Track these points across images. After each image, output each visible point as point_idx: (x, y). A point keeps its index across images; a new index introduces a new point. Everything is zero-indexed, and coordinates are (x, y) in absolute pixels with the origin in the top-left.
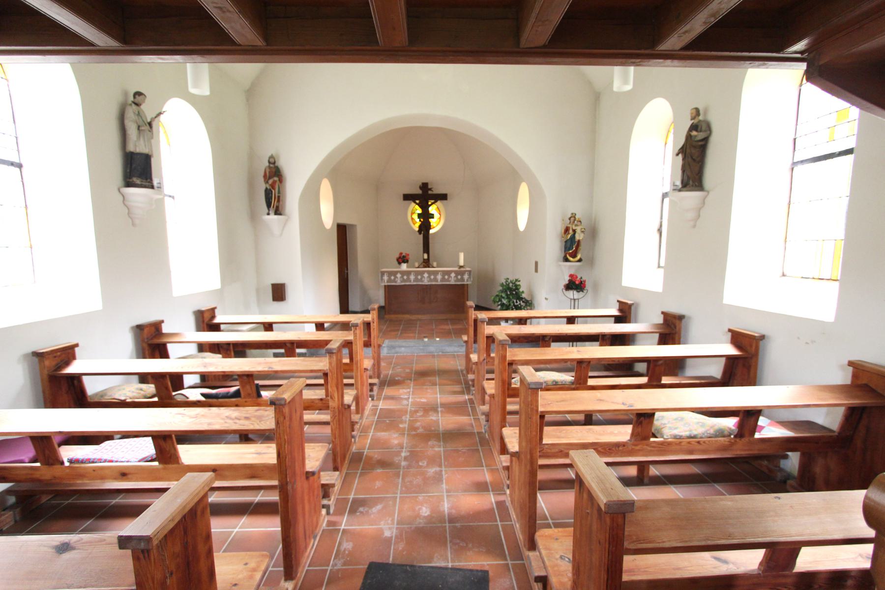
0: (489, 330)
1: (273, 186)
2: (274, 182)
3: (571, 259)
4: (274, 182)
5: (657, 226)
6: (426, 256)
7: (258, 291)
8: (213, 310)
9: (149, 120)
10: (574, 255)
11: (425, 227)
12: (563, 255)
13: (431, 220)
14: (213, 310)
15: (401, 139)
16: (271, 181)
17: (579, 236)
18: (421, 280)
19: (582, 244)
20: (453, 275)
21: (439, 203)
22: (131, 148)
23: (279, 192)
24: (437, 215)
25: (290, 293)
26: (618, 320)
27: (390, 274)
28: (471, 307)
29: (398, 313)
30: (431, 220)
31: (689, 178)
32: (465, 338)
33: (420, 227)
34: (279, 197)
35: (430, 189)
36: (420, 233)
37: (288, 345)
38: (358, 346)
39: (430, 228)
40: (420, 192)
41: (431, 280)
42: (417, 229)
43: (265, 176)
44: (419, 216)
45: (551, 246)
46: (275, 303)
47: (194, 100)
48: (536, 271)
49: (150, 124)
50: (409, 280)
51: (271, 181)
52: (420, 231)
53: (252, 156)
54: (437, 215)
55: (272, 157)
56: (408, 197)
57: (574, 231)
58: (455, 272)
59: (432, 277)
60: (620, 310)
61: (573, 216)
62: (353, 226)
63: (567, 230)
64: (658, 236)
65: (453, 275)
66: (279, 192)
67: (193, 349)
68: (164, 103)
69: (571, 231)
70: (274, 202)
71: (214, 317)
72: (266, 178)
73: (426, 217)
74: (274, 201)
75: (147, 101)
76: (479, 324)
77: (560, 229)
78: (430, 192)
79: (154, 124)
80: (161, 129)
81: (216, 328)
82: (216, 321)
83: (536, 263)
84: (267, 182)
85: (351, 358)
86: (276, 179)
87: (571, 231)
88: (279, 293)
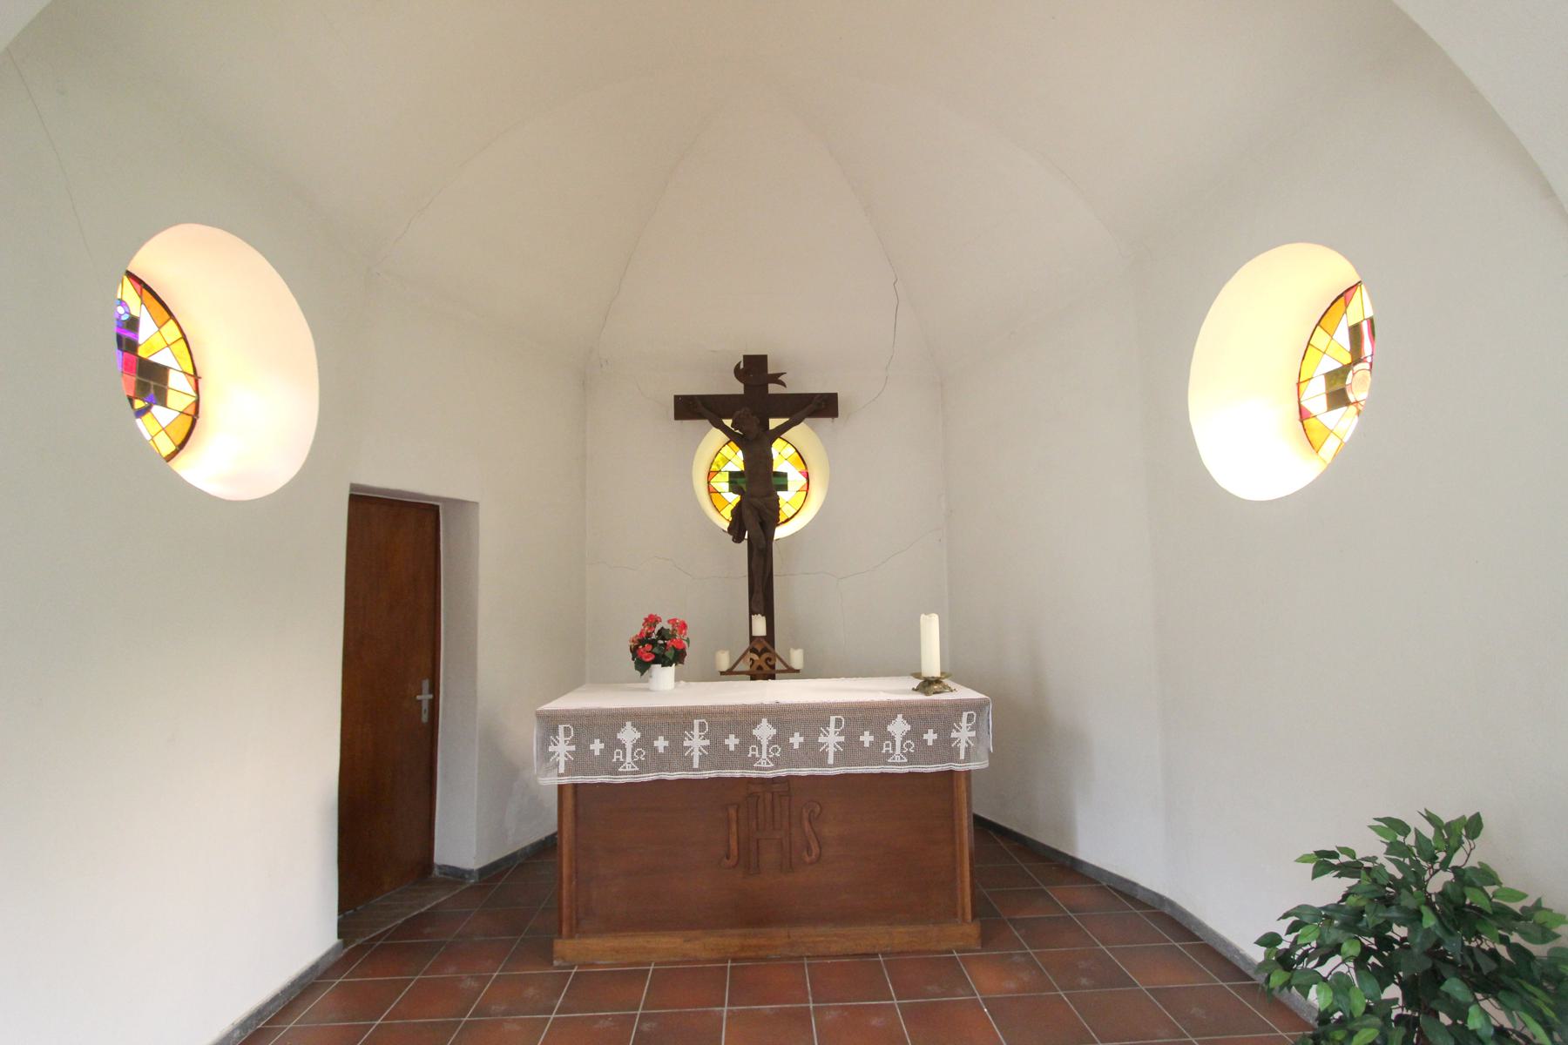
20: (899, 727)
33: (737, 512)
35: (776, 379)
36: (738, 539)
39: (776, 522)
40: (738, 388)
41: (789, 757)
42: (726, 526)
50: (678, 752)
56: (689, 408)
58: (907, 710)
59: (796, 740)
73: (757, 501)
78: (773, 389)
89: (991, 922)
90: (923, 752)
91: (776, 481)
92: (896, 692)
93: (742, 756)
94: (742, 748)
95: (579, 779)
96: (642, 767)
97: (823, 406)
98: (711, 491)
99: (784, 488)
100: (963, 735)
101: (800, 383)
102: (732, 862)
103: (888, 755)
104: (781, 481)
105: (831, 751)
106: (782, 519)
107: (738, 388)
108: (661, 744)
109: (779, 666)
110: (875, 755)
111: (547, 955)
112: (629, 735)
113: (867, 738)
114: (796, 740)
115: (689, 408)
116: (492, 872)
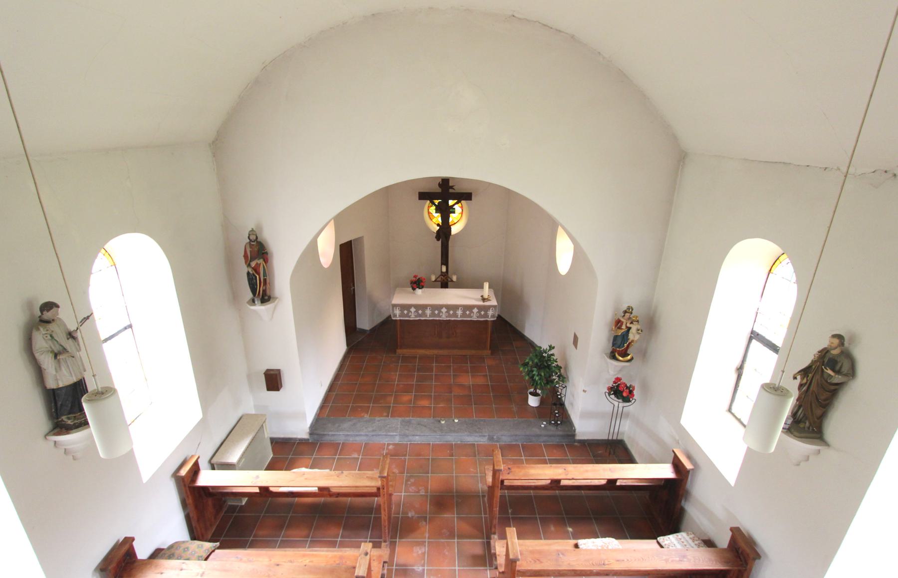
1: (256, 269)
4: (258, 265)
5: (737, 363)
6: (444, 269)
7: (249, 377)
11: (444, 232)
16: (253, 264)
18: (438, 315)
20: (475, 310)
22: (51, 384)
23: (265, 275)
25: (286, 379)
29: (413, 347)
31: (805, 417)
34: (265, 280)
35: (452, 187)
36: (438, 240)
40: (439, 190)
41: (449, 316)
43: (245, 256)
45: (597, 336)
50: (424, 314)
51: (253, 264)
53: (227, 226)
55: (252, 232)
56: (423, 196)
58: (478, 307)
59: (451, 312)
62: (359, 240)
64: (735, 376)
65: (475, 310)
66: (265, 275)
70: (260, 289)
72: (248, 260)
74: (261, 290)
78: (451, 191)
84: (249, 265)
86: (261, 261)
88: (273, 381)
89: (494, 349)
90: (481, 316)
92: (316, 556)
96: (416, 316)
98: (429, 213)
100: (490, 313)
101: (458, 189)
107: (439, 190)
110: (470, 316)
111: (395, 352)
116: (373, 330)
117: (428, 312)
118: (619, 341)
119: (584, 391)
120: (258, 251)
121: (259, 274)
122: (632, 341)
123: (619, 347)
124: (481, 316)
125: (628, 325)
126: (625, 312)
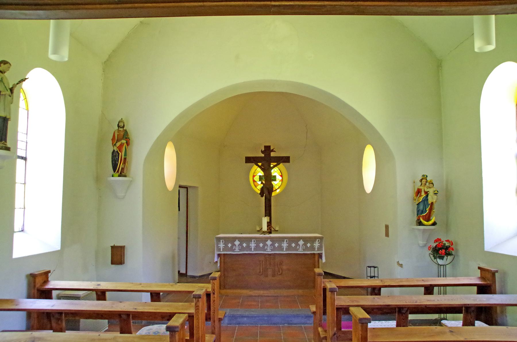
0: (342, 301)
2: (122, 145)
3: (425, 223)
4: (122, 145)
8: (47, 273)
9: (11, 86)
10: (428, 219)
11: (267, 190)
12: (416, 218)
13: (273, 183)
14: (47, 273)
15: (249, 103)
16: (118, 144)
17: (431, 199)
19: (435, 206)
21: (281, 165)
23: (125, 155)
24: (279, 178)
26: (483, 289)
27: (227, 240)
28: (320, 275)
30: (273, 183)
32: (313, 308)
33: (262, 189)
34: (125, 159)
36: (262, 196)
37: (124, 317)
38: (200, 321)
39: (272, 191)
42: (259, 192)
44: (261, 178)
46: (113, 266)
47: (54, 69)
48: (387, 235)
49: (12, 90)
52: (262, 194)
54: (279, 178)
56: (249, 160)
57: (427, 193)
60: (482, 278)
61: (425, 177)
63: (419, 192)
67: (18, 320)
68: (28, 72)
69: (423, 193)
70: (120, 166)
71: (46, 281)
73: (268, 178)
74: (119, 164)
75: (11, 69)
76: (328, 294)
77: (411, 192)
79: (15, 91)
80: (22, 104)
81: (46, 294)
82: (50, 286)
83: (387, 227)
85: (192, 335)
86: (124, 141)
87: (423, 193)
88: (118, 256)
91: (272, 178)
93: (231, 249)
94: (264, 246)
95: (225, 253)
97: (286, 160)
98: (254, 181)
99: (275, 180)
102: (261, 273)
103: (235, 249)
104: (233, 315)
105: (316, 247)
106: (274, 189)
108: (245, 245)
109: (272, 229)
110: (231, 249)
112: (237, 243)
113: (293, 245)
114: (276, 245)
115: (249, 160)
117: (253, 245)
118: (421, 207)
119: (401, 265)
120: (122, 137)
121: (121, 152)
122: (432, 203)
123: (422, 212)
124: (307, 248)
125: (426, 190)
126: (421, 181)
